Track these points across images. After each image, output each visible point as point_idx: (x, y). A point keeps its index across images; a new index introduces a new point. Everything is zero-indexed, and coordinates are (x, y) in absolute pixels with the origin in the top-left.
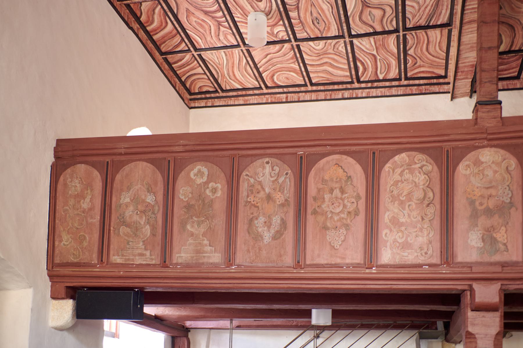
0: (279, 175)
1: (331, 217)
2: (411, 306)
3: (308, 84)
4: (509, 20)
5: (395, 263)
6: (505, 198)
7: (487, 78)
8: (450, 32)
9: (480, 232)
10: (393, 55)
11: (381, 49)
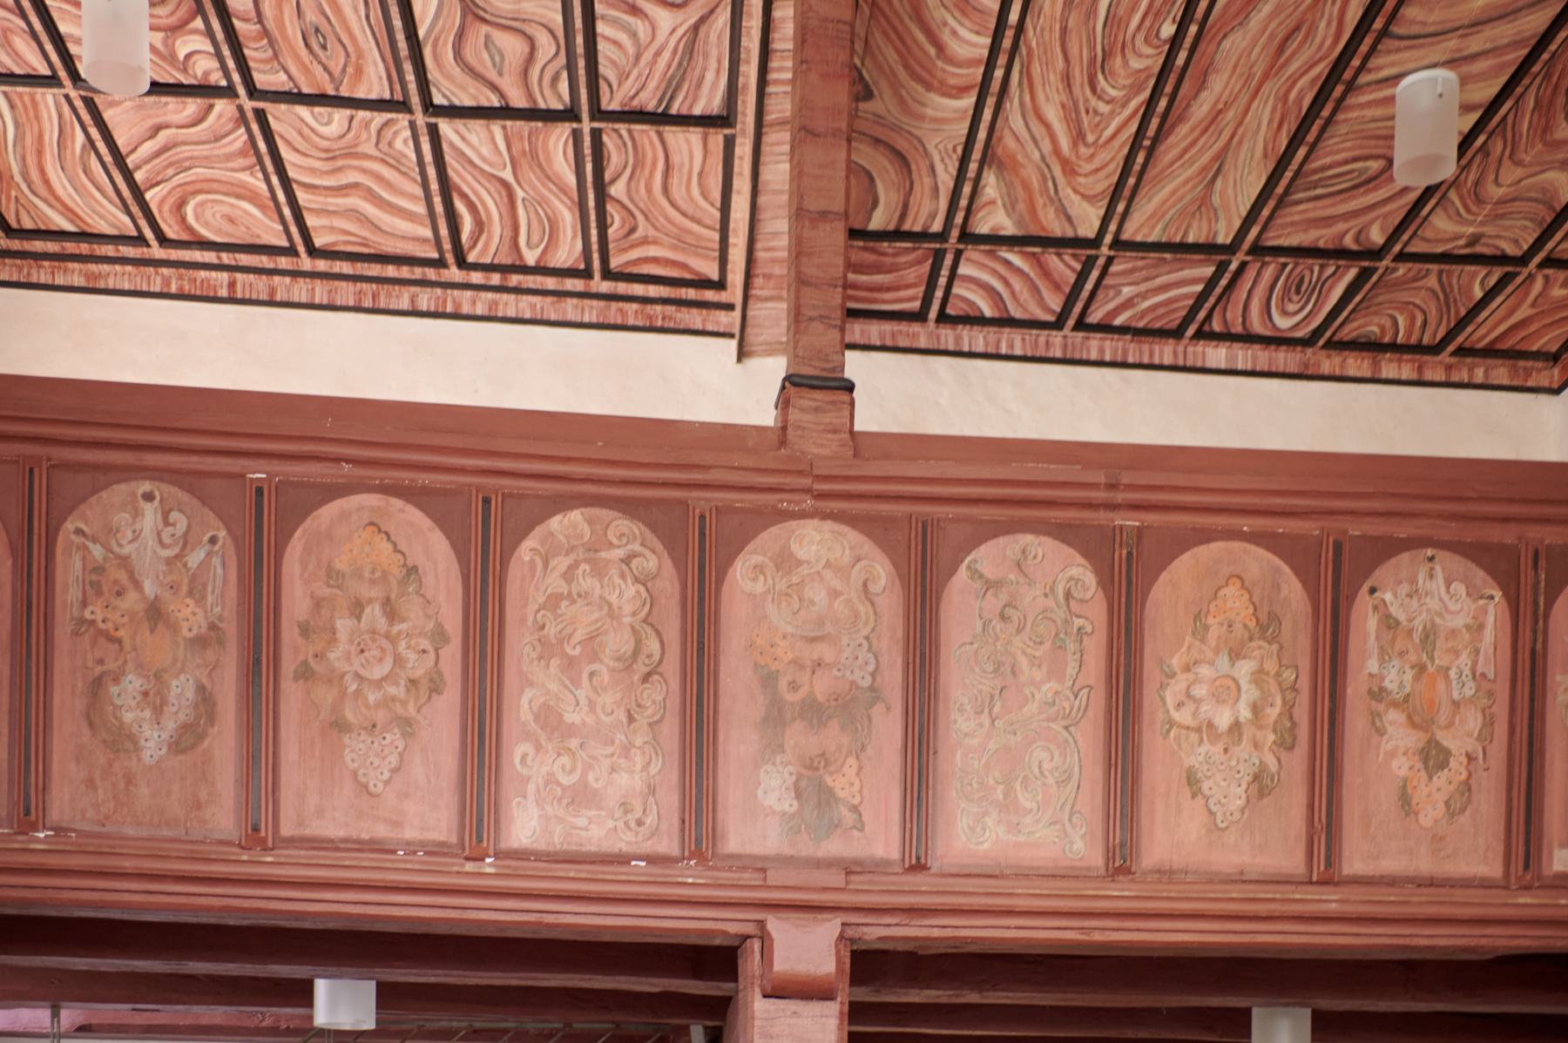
0: (186, 542)
1: (358, 692)
2: (608, 978)
3: (301, 249)
4: (893, 135)
5: (551, 849)
6: (857, 676)
7: (814, 307)
8: (729, 144)
9: (791, 768)
10: (563, 190)
11: (525, 166)
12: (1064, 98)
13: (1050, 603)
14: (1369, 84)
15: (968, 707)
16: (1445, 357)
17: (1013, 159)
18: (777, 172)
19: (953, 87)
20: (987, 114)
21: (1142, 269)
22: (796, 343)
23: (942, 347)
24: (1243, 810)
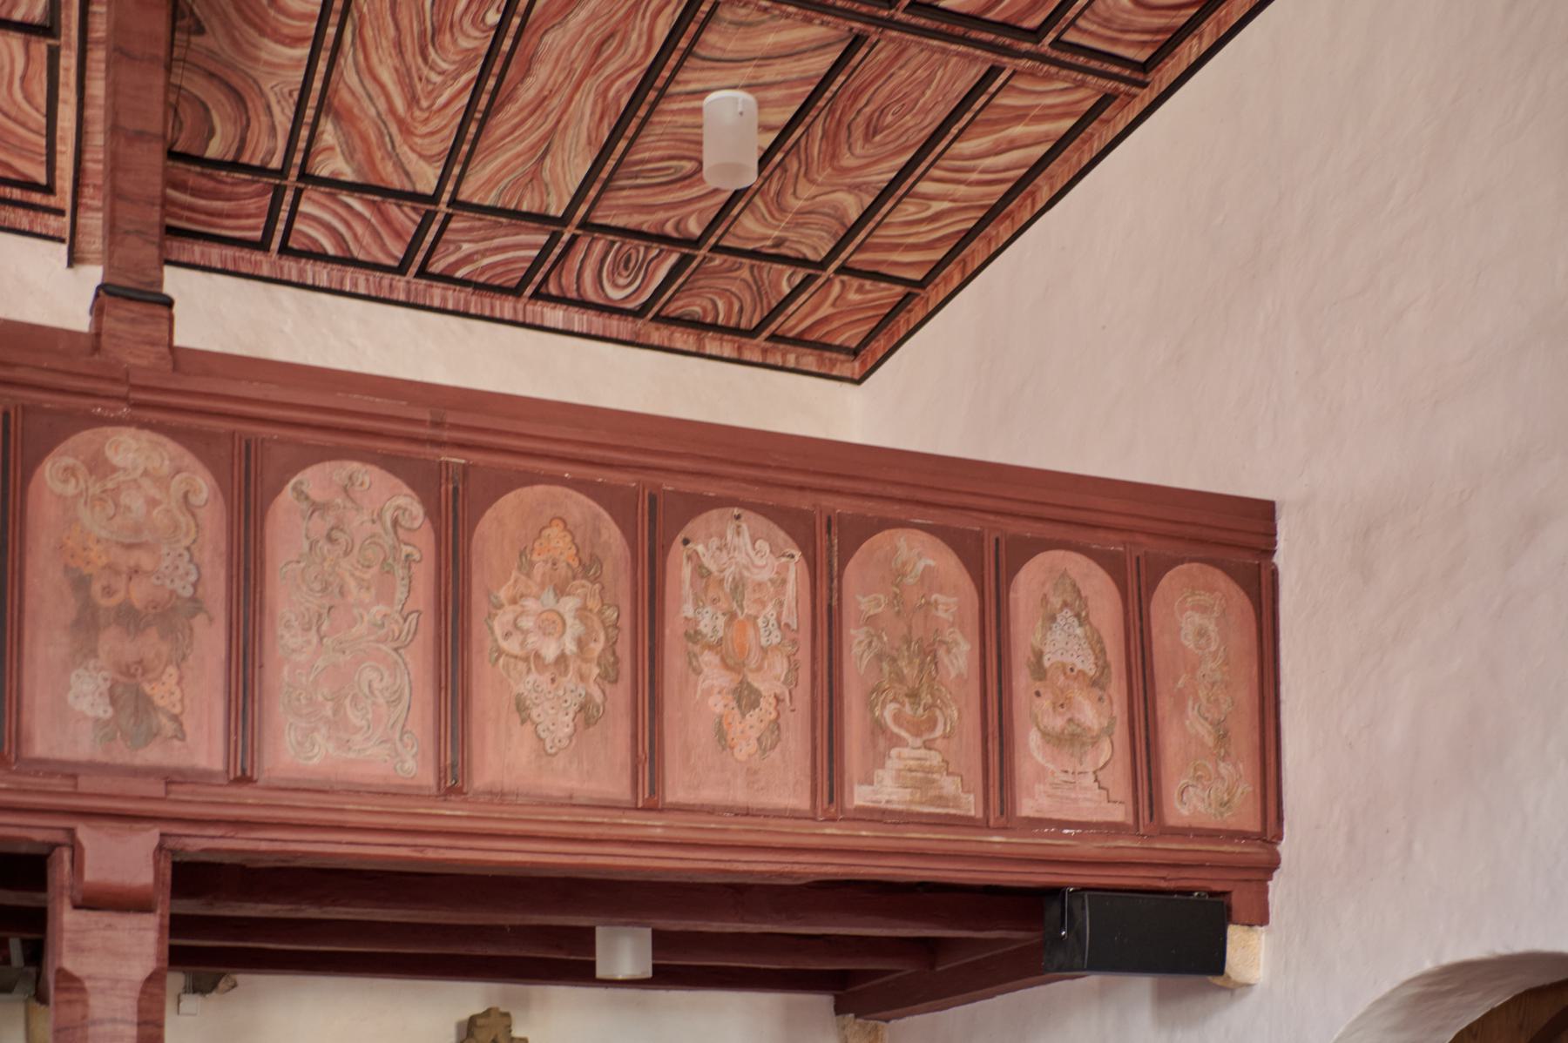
6: (178, 584)
8: (54, 55)
9: (105, 674)
12: (397, 62)
13: (378, 528)
14: (679, 94)
15: (296, 624)
16: (760, 340)
17: (350, 111)
18: (97, 88)
19: (287, 36)
20: (322, 67)
21: (480, 229)
22: (111, 257)
23: (285, 277)
24: (570, 738)
